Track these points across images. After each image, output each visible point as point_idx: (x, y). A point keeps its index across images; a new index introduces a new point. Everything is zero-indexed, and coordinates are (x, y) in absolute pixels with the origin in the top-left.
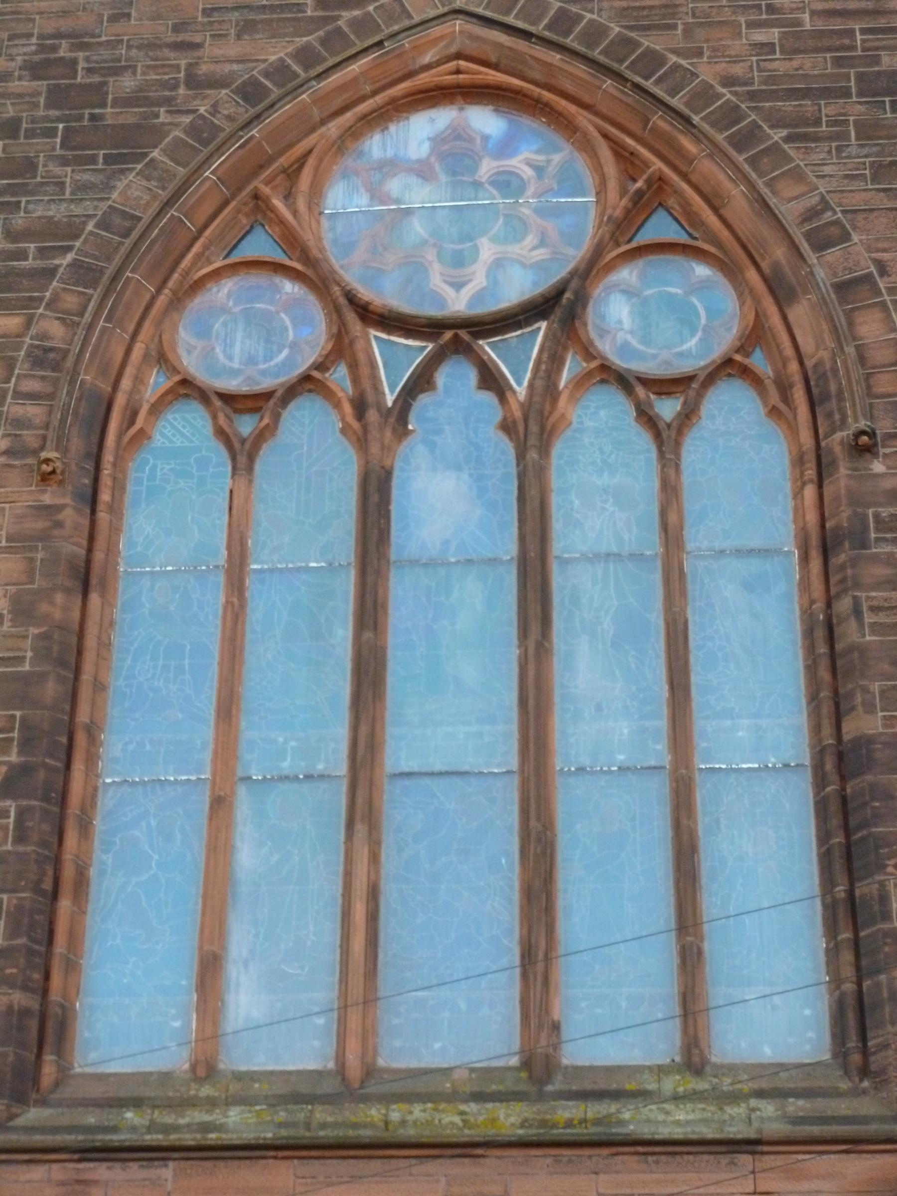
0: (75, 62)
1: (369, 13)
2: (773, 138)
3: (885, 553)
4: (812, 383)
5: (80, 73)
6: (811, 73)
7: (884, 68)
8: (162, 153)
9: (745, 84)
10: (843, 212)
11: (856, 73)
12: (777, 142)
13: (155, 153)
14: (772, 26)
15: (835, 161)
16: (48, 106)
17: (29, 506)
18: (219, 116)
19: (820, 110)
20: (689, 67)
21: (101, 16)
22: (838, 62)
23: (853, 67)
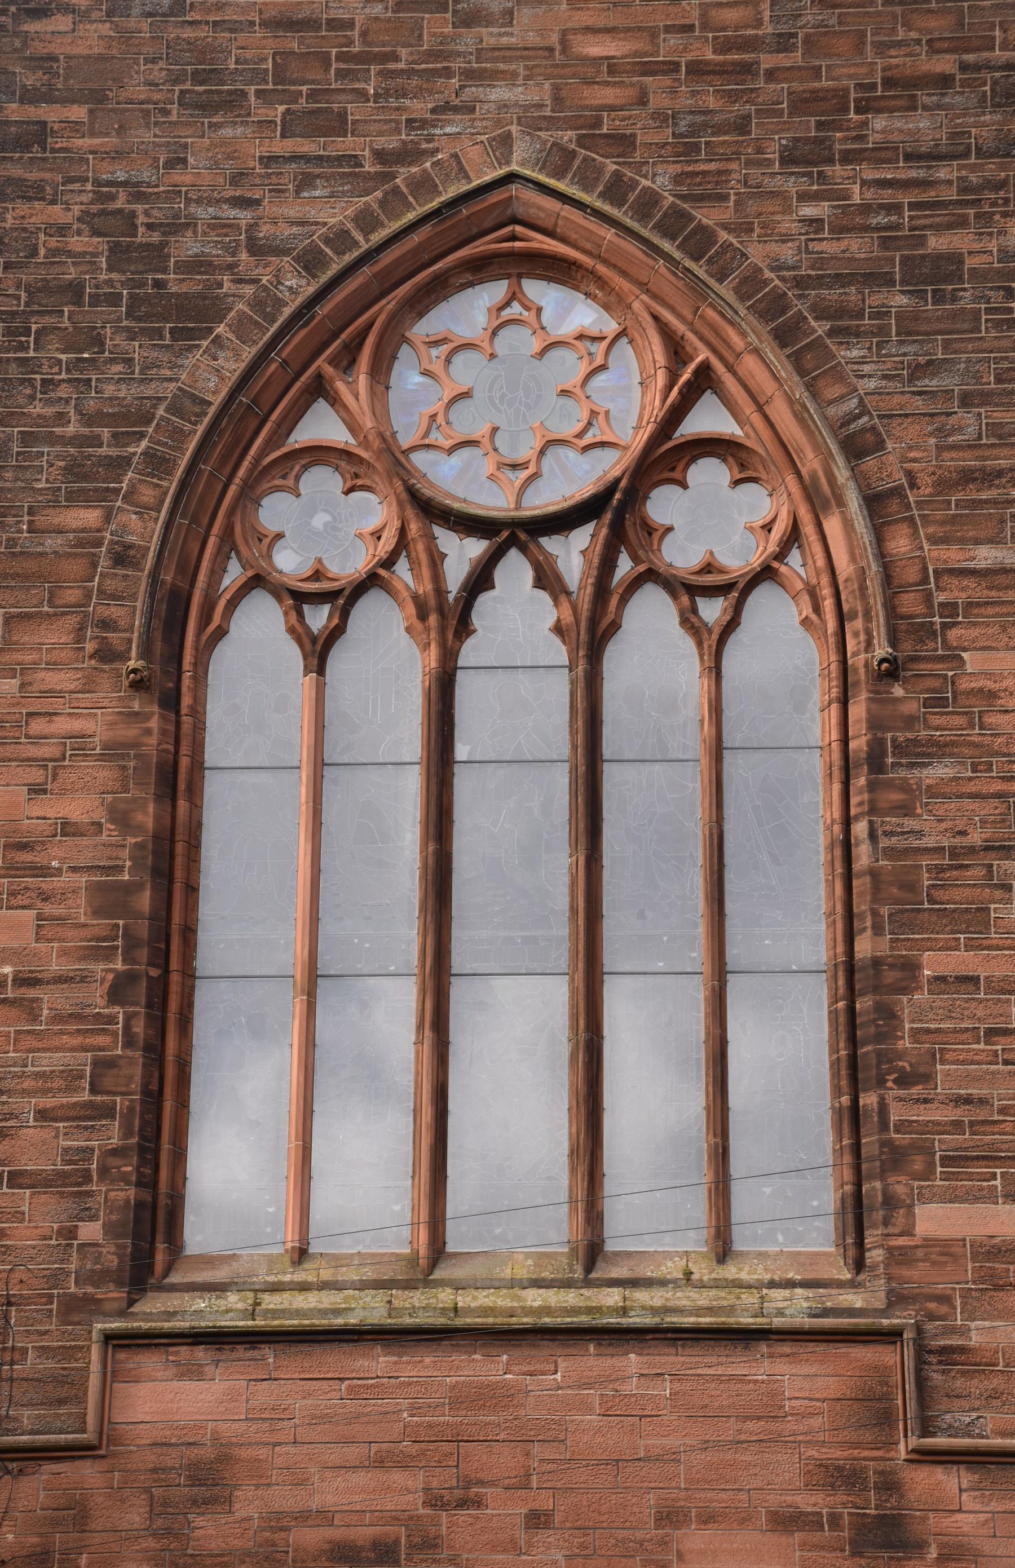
0: (133, 214)
1: (425, 170)
2: (817, 331)
3: (900, 778)
4: (843, 597)
5: (141, 230)
6: (857, 256)
7: (930, 251)
8: (227, 329)
9: (793, 268)
10: (879, 416)
11: (902, 256)
12: (820, 336)
13: (221, 329)
14: (824, 200)
15: (875, 359)
16: (110, 269)
17: (120, 713)
18: (281, 288)
19: (864, 301)
20: (739, 246)
21: (156, 160)
22: (885, 243)
23: (898, 249)
